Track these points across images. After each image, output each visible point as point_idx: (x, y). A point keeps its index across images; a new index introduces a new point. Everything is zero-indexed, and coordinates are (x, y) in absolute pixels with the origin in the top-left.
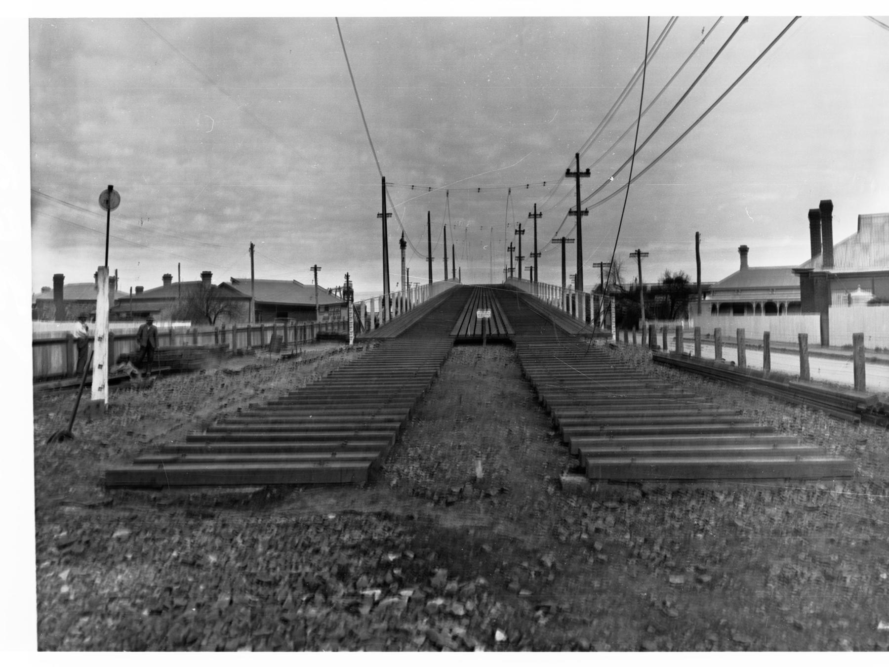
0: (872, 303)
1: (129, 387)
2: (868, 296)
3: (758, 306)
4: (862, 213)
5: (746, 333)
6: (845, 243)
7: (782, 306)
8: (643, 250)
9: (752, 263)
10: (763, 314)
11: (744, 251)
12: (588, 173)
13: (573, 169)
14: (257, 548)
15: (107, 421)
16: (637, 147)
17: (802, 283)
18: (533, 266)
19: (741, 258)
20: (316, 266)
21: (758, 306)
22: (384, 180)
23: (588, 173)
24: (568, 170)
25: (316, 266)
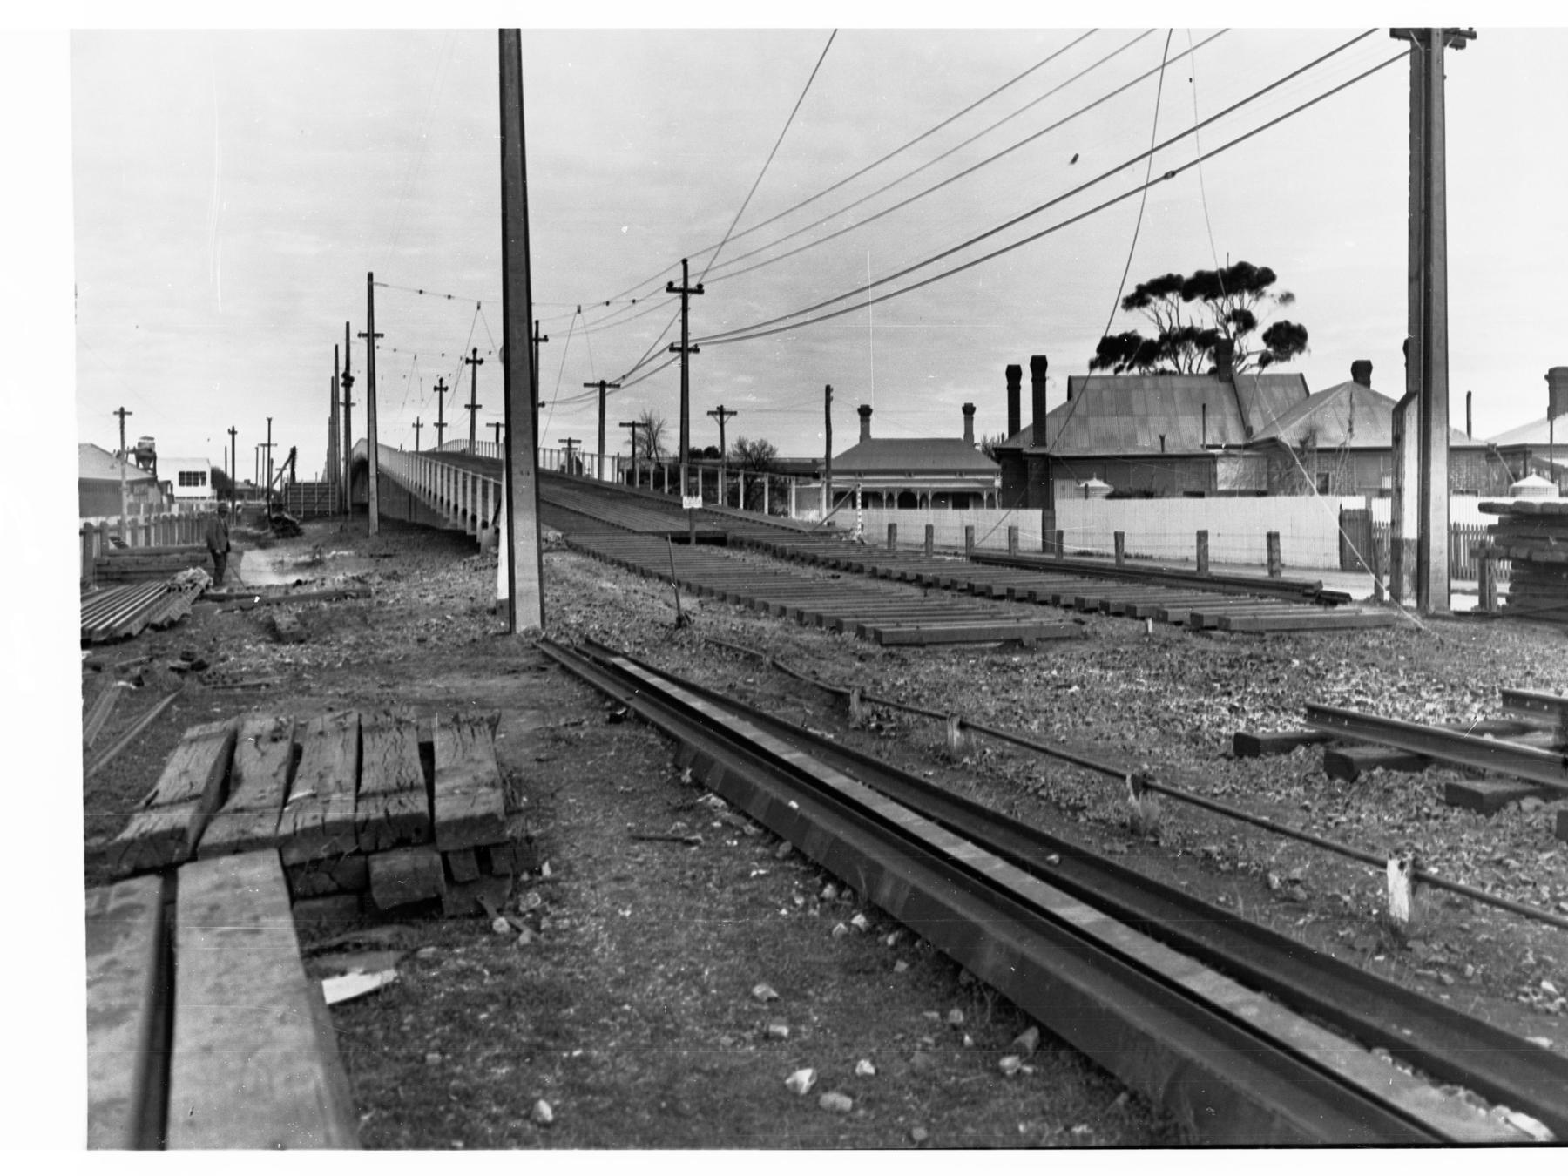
0: (1110, 497)
1: (1210, 637)
2: (1108, 488)
3: (890, 497)
4: (1073, 374)
5: (1020, 533)
6: (1054, 412)
7: (924, 496)
8: (727, 408)
9: (875, 433)
10: (1317, 495)
11: (969, 410)
12: (699, 290)
13: (678, 284)
14: (503, 1067)
15: (1504, 812)
16: (713, 266)
17: (309, 487)
18: (502, 420)
19: (966, 419)
20: (122, 409)
21: (890, 497)
22: (370, 276)
23: (699, 290)
24: (671, 284)
25: (122, 409)
